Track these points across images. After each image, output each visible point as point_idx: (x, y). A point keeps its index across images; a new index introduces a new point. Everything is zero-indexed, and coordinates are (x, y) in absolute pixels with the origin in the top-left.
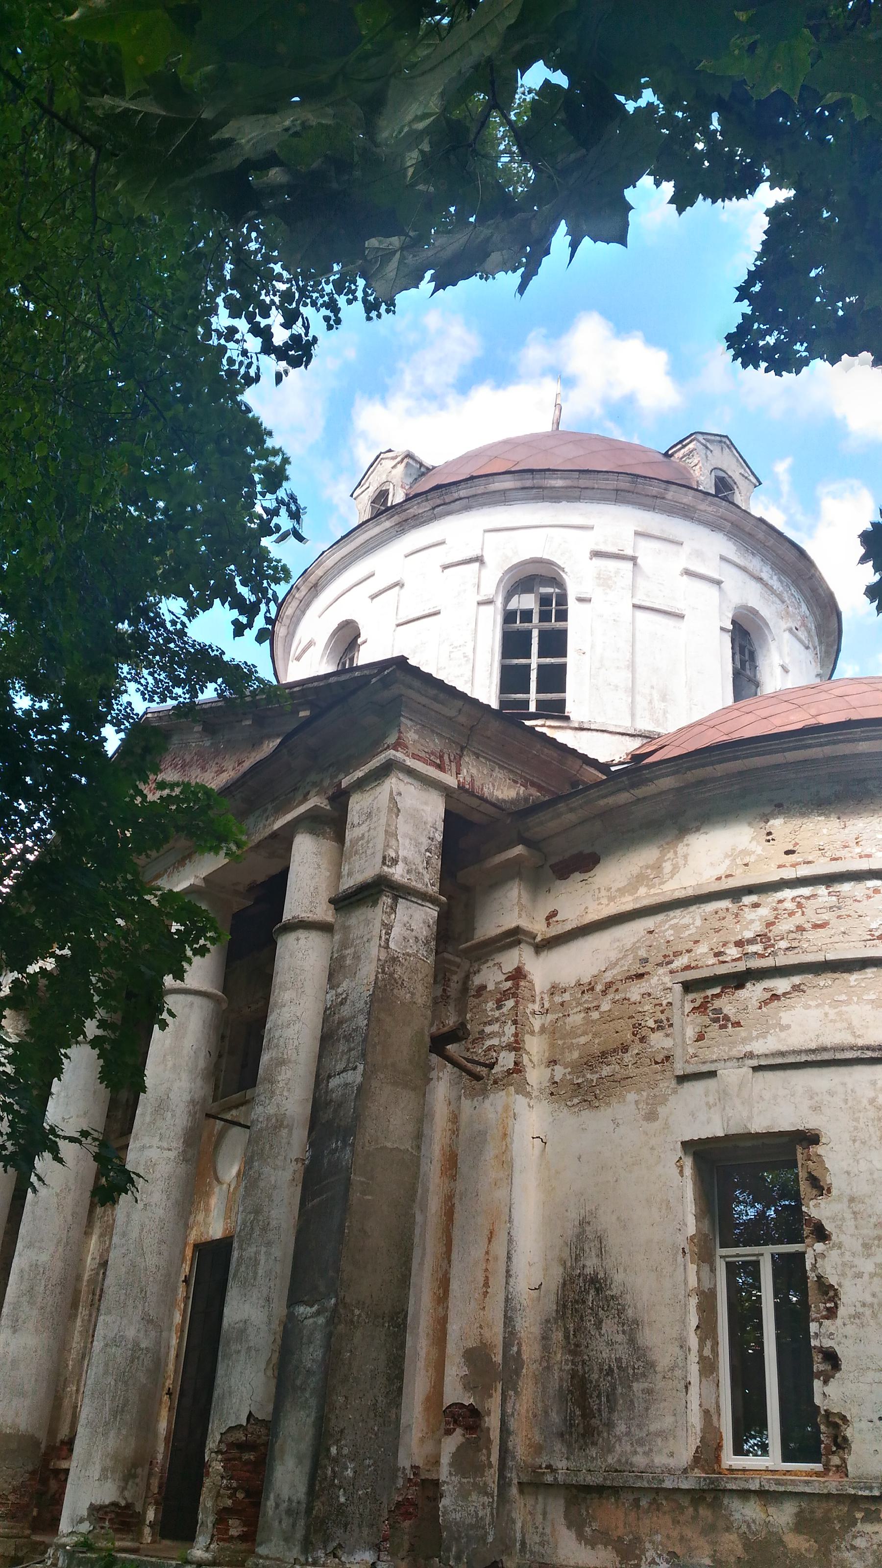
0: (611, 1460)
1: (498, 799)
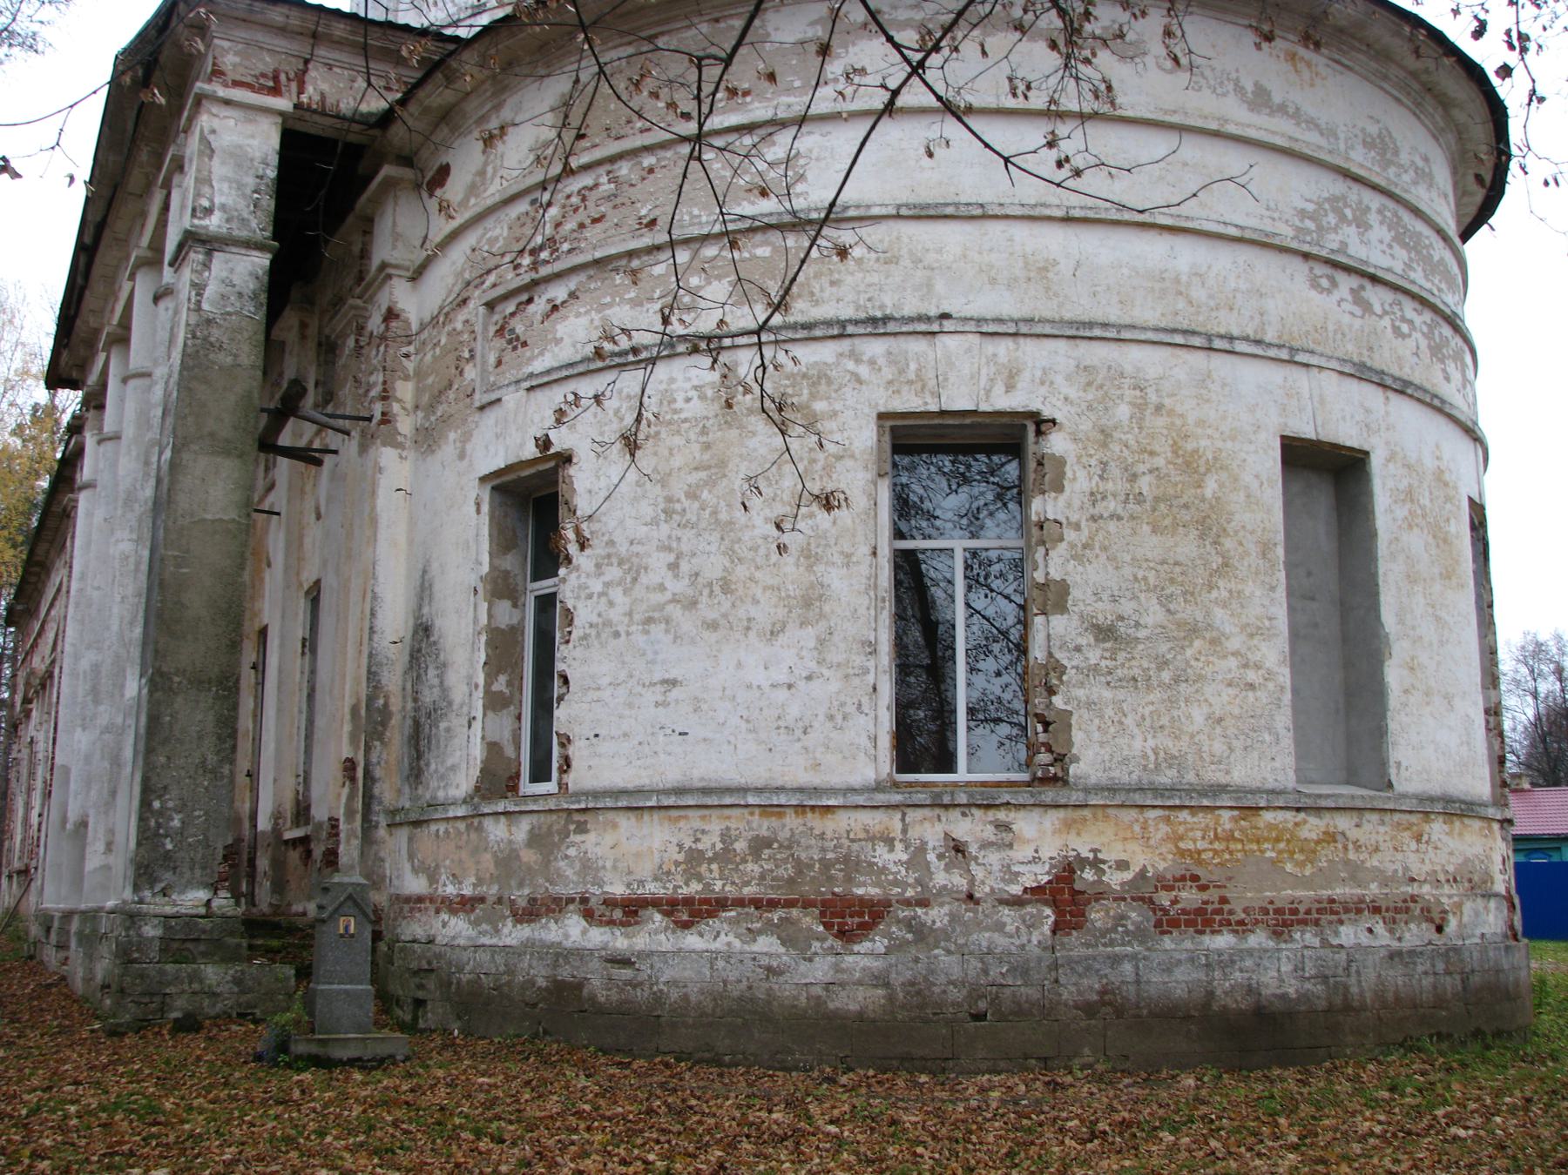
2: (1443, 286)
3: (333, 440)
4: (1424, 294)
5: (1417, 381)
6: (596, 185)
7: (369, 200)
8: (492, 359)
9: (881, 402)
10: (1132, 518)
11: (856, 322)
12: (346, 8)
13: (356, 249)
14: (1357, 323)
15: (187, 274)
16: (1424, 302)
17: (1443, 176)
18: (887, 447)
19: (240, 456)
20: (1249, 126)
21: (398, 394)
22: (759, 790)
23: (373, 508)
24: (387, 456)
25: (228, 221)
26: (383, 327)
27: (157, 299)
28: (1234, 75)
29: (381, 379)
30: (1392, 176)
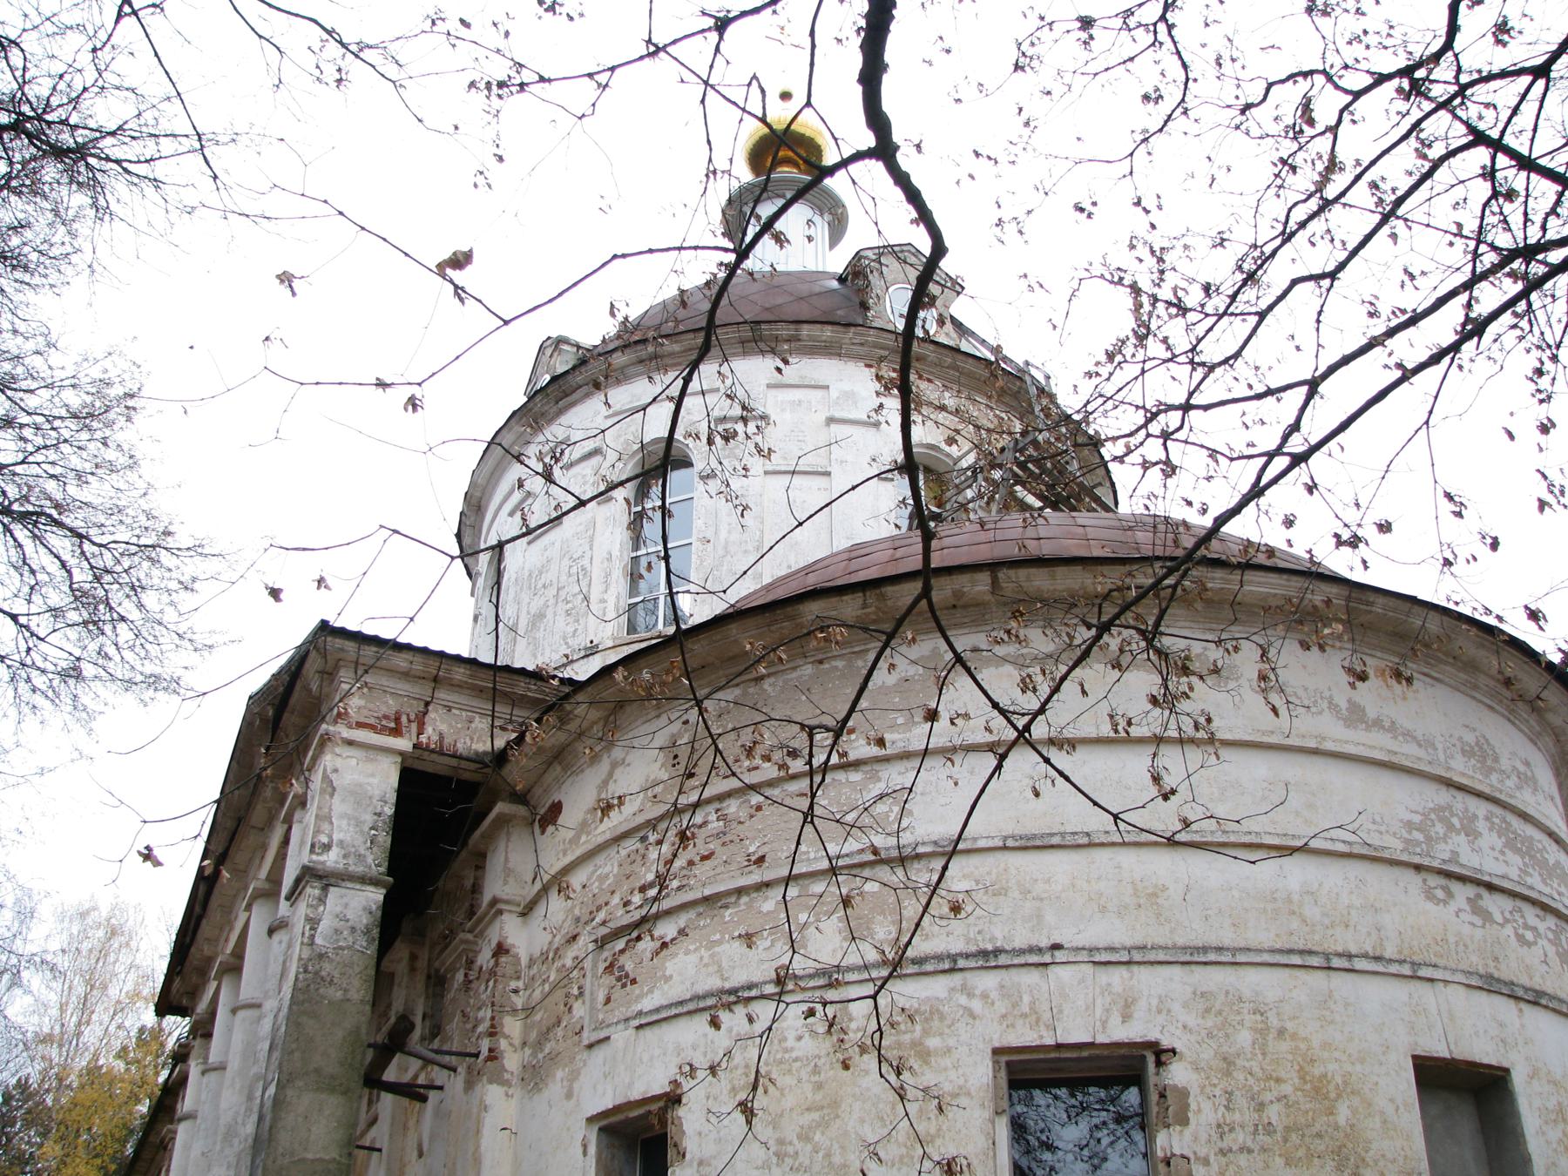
1: (477, 753)
2: (1563, 889)
3: (439, 1076)
4: (1545, 900)
5: (1549, 991)
6: (705, 823)
7: (482, 836)
8: (601, 997)
9: (996, 1037)
10: (1264, 1150)
11: (967, 956)
12: (465, 654)
13: (468, 883)
14: (1479, 933)
15: (302, 908)
16: (1545, 908)
17: (1545, 776)
18: (1004, 1083)
19: (344, 1093)
20: (1346, 742)
21: (506, 1030)
23: (478, 1147)
24: (493, 1093)
25: (345, 856)
26: (492, 962)
27: (271, 932)
28: (1327, 694)
29: (489, 1014)
30: (1495, 782)
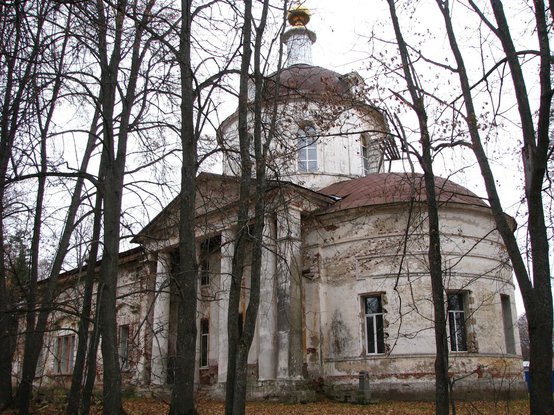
0: (344, 356)
22: (431, 354)
